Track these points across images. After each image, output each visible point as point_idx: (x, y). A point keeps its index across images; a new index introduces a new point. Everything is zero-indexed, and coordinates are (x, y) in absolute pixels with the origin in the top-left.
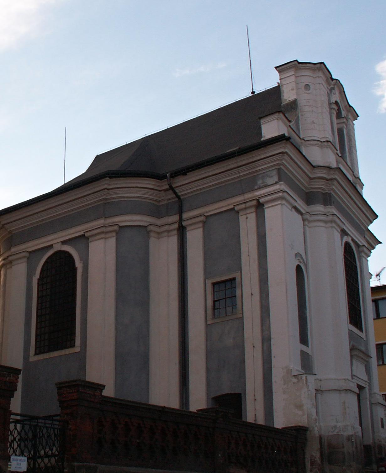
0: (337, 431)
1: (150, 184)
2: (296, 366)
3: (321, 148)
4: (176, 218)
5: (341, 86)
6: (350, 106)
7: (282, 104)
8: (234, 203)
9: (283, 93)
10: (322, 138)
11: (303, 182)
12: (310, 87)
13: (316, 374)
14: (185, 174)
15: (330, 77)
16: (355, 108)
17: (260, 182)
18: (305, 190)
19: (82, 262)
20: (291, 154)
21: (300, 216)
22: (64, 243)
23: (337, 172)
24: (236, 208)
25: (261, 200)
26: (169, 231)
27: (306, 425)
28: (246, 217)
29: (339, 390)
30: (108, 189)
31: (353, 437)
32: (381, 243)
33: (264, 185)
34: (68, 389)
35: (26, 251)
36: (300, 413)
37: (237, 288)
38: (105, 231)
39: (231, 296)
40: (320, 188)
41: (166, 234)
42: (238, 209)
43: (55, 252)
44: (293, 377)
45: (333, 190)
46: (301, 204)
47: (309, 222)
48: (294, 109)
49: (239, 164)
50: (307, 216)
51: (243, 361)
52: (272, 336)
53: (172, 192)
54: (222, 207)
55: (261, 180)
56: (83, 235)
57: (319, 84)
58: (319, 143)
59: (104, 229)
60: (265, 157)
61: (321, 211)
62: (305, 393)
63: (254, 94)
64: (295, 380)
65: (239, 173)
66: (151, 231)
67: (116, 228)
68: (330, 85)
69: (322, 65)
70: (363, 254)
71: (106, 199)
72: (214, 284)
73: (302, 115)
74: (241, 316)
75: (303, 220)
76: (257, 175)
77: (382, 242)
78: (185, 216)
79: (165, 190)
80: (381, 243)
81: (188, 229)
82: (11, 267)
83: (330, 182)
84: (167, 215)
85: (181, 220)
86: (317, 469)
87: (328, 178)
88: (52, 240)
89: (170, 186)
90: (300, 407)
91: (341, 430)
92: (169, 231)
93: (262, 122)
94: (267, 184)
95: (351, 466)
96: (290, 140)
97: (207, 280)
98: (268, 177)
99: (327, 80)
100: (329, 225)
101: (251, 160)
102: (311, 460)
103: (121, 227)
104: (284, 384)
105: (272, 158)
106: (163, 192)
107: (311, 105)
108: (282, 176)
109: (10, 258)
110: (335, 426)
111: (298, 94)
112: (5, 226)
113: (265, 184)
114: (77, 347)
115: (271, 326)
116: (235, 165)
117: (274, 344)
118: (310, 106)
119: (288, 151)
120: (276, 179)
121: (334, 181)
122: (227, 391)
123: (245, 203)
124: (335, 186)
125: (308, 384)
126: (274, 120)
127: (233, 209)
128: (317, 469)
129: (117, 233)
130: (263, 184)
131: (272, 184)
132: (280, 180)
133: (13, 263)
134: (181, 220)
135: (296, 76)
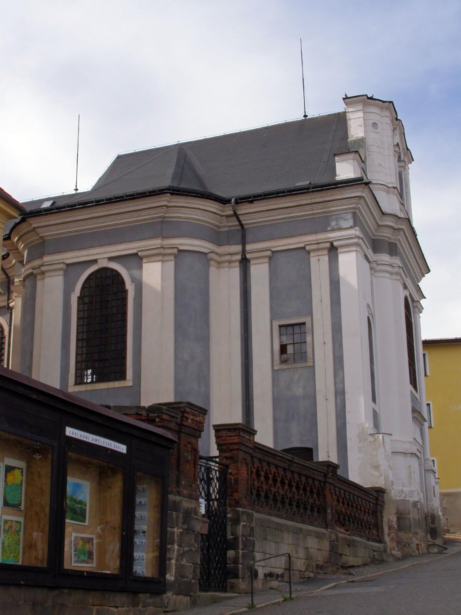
0: (403, 496)
1: (212, 207)
2: (369, 425)
3: (388, 194)
4: (238, 248)
5: (402, 127)
6: (408, 149)
7: (349, 140)
8: (305, 242)
9: (350, 128)
10: (388, 183)
11: (372, 228)
12: (377, 125)
13: (392, 435)
14: (252, 202)
15: (396, 117)
16: (411, 151)
17: (333, 223)
18: (371, 236)
19: (134, 284)
20: (367, 200)
21: (367, 264)
22: (111, 259)
23: (405, 223)
24: (307, 248)
25: (335, 244)
26: (230, 262)
27: (383, 486)
28: (318, 259)
29: (405, 453)
30: (168, 207)
31: (419, 503)
32: (425, 298)
33: (337, 228)
34: (228, 433)
35: (64, 262)
36: (377, 474)
37: (307, 333)
38: (163, 253)
39: (300, 342)
40: (386, 237)
41: (227, 264)
42: (309, 249)
43: (100, 268)
44: (370, 436)
45: (399, 240)
46: (370, 253)
47: (376, 271)
48: (363, 148)
49: (313, 201)
50: (374, 265)
51: (315, 414)
52: (346, 390)
53: (236, 219)
54: (291, 244)
55: (335, 222)
56: (136, 254)
57: (387, 124)
58: (386, 188)
59: (161, 251)
60: (341, 198)
61: (387, 262)
62: (382, 453)
63: (306, 118)
64: (371, 439)
65: (313, 210)
66: (211, 259)
67: (175, 251)
68: (394, 126)
69: (391, 104)
70: (417, 310)
71: (164, 217)
72: (280, 326)
73: (369, 155)
74: (311, 364)
75: (371, 269)
76: (331, 215)
77: (426, 298)
78: (249, 247)
79: (227, 216)
80: (425, 298)
81: (252, 262)
82: (43, 279)
83: (396, 232)
84: (229, 243)
85: (244, 252)
86: (394, 534)
87: (397, 227)
88: (97, 254)
89: (234, 213)
90: (377, 467)
91: (407, 496)
92: (230, 262)
93: (337, 160)
94: (341, 227)
95: (416, 533)
96: (369, 185)
97: (273, 321)
98: (343, 220)
99: (392, 121)
100: (395, 277)
101: (326, 199)
102: (388, 523)
103: (180, 251)
104: (360, 443)
105: (348, 201)
106: (224, 217)
107: (378, 146)
108: (357, 222)
109: (43, 269)
110: (402, 491)
111: (365, 132)
112: (36, 230)
113: (339, 226)
114: (128, 380)
115: (345, 378)
116: (309, 202)
117: (348, 399)
118: (377, 146)
119: (365, 196)
120: (351, 223)
121: (401, 231)
122: (296, 444)
123: (318, 243)
124: (401, 237)
125: (385, 444)
126: (350, 159)
127: (304, 248)
128: (394, 534)
129: (176, 256)
130: (337, 227)
131: (347, 227)
132: (355, 225)
133: (46, 275)
134: (244, 252)
135: (365, 111)
